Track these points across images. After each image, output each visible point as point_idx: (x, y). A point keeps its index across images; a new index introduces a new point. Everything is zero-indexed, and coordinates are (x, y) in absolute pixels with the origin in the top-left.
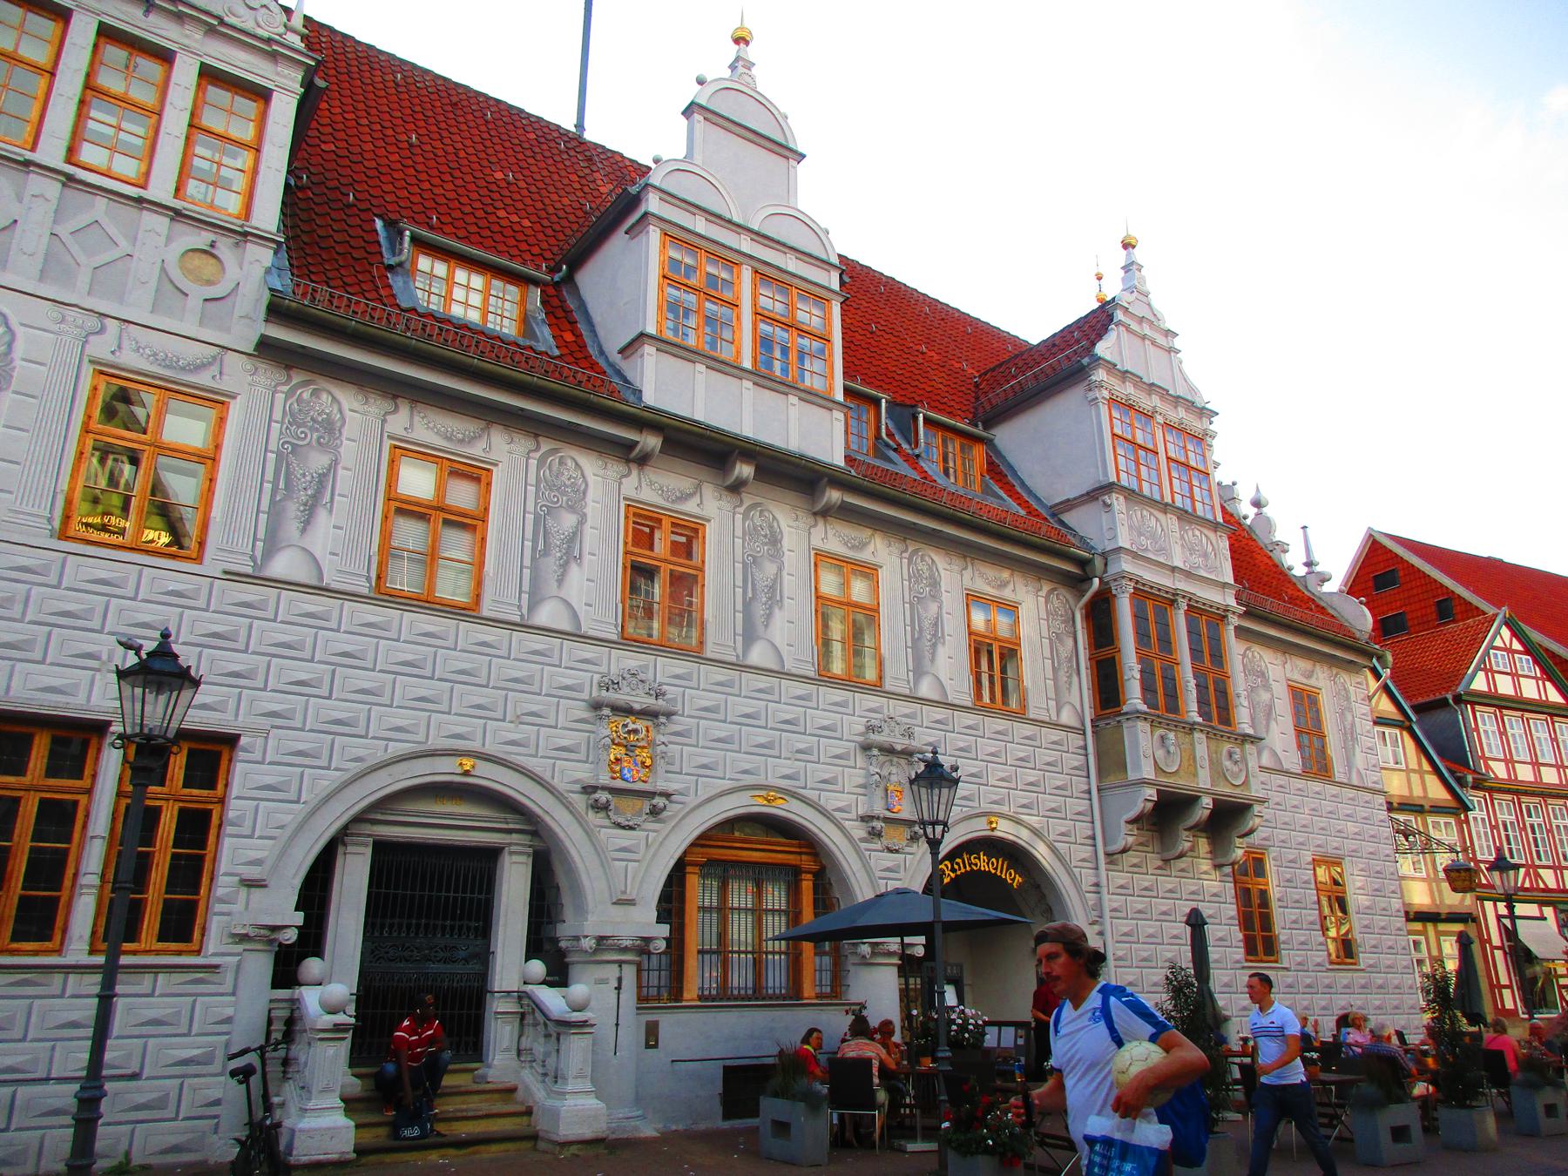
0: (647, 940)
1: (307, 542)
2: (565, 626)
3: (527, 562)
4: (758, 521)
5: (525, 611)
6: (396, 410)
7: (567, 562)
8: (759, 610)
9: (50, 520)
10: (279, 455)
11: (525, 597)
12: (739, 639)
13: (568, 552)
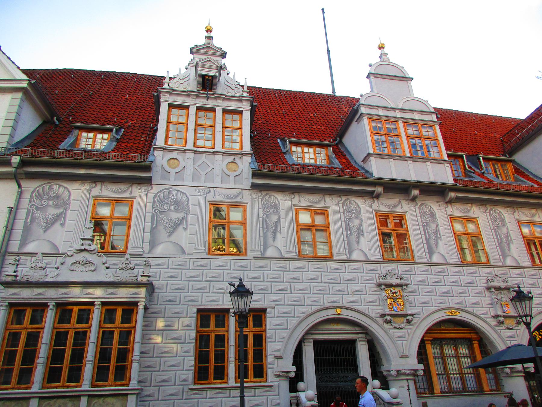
0: (416, 371)
3: (345, 239)
5: (348, 255)
6: (448, 206)
7: (437, 240)
8: (432, 242)
9: (205, 250)
11: (347, 250)
12: (427, 254)
13: (359, 233)
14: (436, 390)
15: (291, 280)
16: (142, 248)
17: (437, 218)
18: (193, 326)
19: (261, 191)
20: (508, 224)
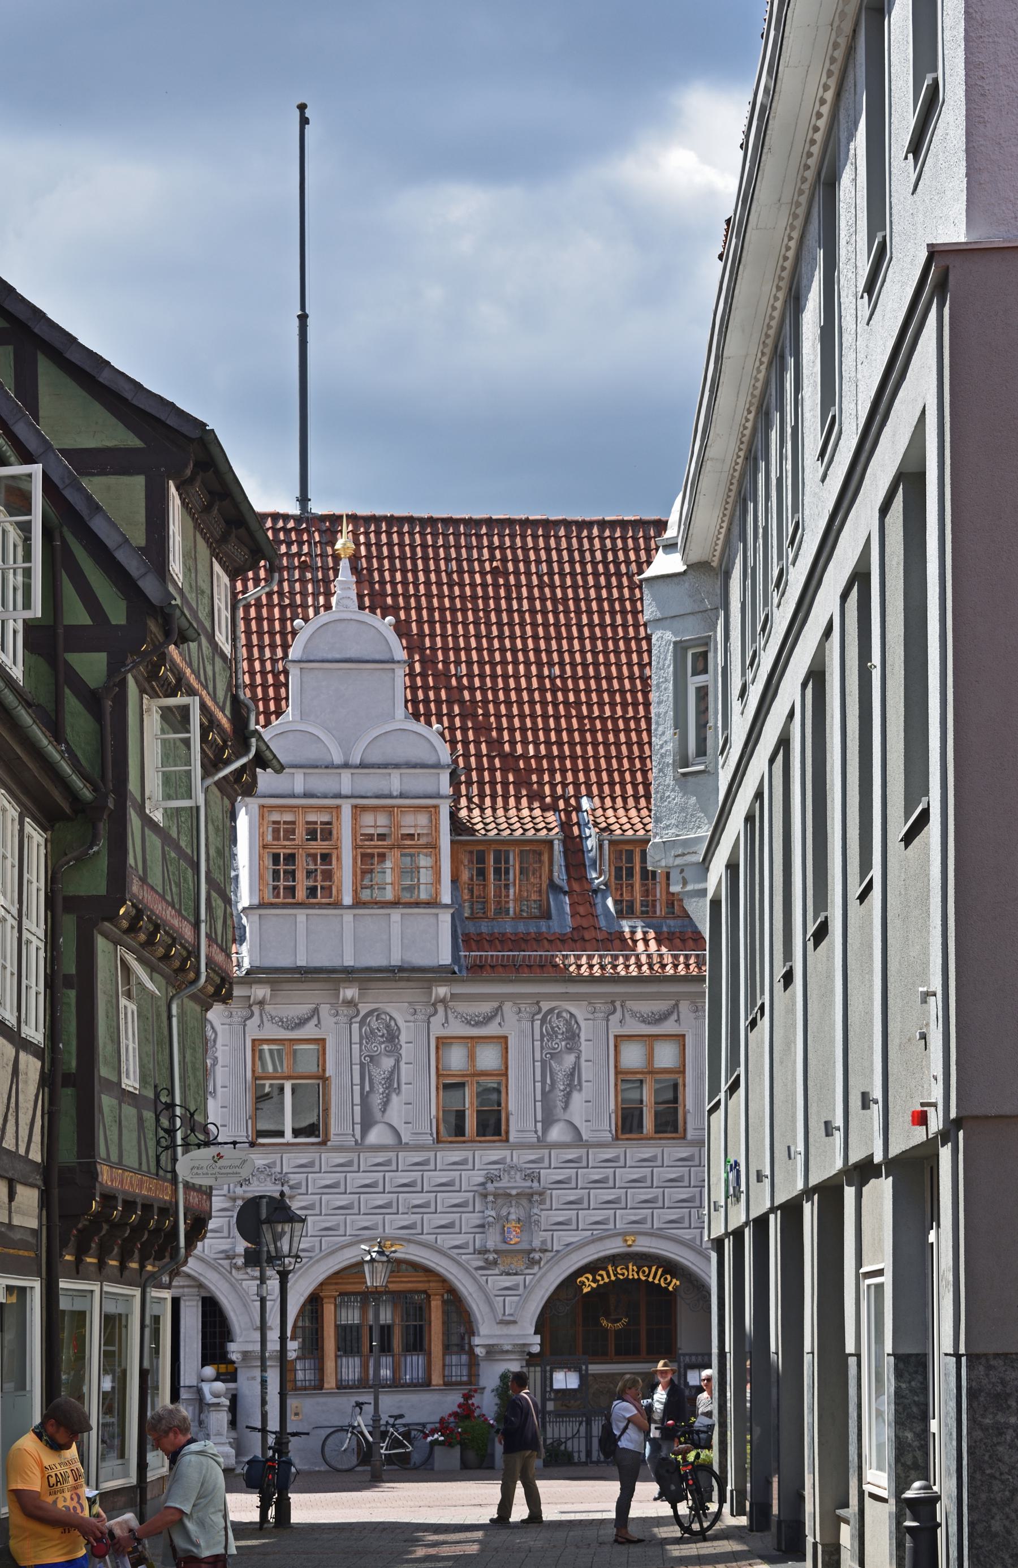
4: (374, 1024)
8: (376, 1100)
10: (362, 1065)
12: (358, 1127)
14: (329, 1383)
17: (402, 1043)
20: (584, 1046)
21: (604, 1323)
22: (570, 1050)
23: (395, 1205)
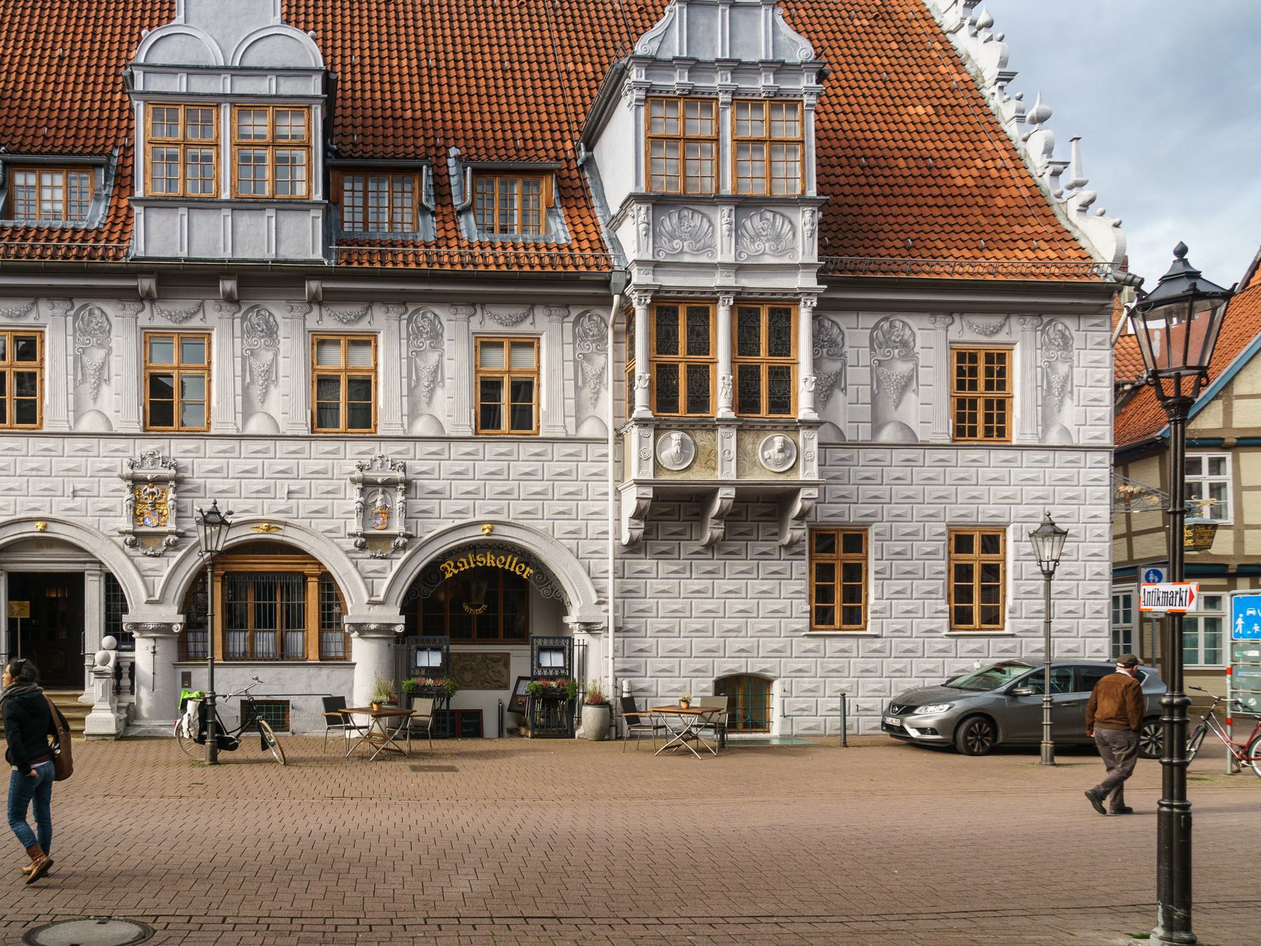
0: (170, 625)
1: (266, 407)
2: (102, 429)
3: (71, 390)
5: (72, 423)
6: (311, 310)
7: (99, 385)
8: (256, 392)
10: (243, 357)
11: (71, 414)
12: (239, 416)
15: (29, 473)
16: (565, 427)
18: (942, 553)
19: (404, 303)
21: (466, 608)
22: (434, 348)
23: (272, 489)
